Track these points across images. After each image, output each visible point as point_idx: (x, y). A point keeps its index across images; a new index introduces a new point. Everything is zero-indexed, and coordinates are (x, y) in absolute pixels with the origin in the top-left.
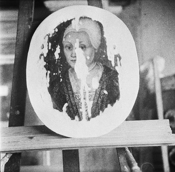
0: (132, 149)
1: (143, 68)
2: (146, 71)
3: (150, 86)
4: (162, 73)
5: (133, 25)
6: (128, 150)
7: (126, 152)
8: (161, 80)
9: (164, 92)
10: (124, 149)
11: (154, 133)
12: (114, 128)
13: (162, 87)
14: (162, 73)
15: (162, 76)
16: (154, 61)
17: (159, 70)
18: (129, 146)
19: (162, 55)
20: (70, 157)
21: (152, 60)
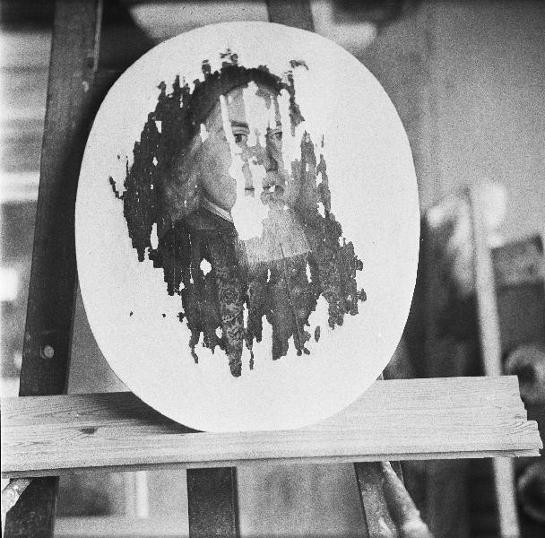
0: (402, 467)
1: (436, 218)
2: (449, 227)
3: (462, 274)
4: (498, 230)
5: (402, 80)
6: (389, 470)
7: (384, 475)
8: (495, 253)
9: (502, 290)
10: (378, 466)
11: (476, 417)
12: (333, 397)
13: (498, 274)
14: (498, 230)
15: (497, 241)
16: (474, 195)
17: (488, 223)
18: (189, 467)
19: (497, 177)
20: (212, 490)
21: (465, 193)
